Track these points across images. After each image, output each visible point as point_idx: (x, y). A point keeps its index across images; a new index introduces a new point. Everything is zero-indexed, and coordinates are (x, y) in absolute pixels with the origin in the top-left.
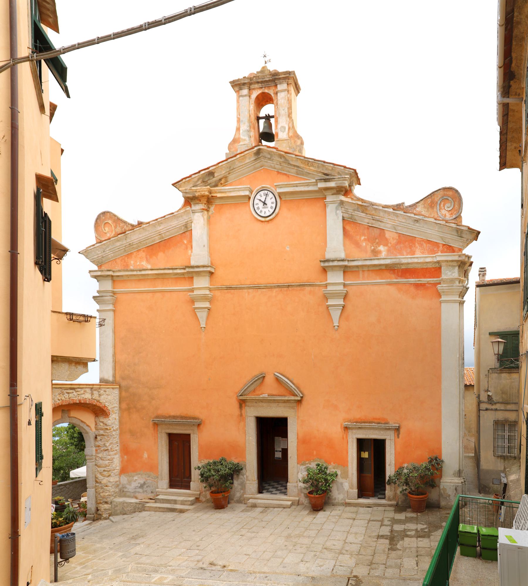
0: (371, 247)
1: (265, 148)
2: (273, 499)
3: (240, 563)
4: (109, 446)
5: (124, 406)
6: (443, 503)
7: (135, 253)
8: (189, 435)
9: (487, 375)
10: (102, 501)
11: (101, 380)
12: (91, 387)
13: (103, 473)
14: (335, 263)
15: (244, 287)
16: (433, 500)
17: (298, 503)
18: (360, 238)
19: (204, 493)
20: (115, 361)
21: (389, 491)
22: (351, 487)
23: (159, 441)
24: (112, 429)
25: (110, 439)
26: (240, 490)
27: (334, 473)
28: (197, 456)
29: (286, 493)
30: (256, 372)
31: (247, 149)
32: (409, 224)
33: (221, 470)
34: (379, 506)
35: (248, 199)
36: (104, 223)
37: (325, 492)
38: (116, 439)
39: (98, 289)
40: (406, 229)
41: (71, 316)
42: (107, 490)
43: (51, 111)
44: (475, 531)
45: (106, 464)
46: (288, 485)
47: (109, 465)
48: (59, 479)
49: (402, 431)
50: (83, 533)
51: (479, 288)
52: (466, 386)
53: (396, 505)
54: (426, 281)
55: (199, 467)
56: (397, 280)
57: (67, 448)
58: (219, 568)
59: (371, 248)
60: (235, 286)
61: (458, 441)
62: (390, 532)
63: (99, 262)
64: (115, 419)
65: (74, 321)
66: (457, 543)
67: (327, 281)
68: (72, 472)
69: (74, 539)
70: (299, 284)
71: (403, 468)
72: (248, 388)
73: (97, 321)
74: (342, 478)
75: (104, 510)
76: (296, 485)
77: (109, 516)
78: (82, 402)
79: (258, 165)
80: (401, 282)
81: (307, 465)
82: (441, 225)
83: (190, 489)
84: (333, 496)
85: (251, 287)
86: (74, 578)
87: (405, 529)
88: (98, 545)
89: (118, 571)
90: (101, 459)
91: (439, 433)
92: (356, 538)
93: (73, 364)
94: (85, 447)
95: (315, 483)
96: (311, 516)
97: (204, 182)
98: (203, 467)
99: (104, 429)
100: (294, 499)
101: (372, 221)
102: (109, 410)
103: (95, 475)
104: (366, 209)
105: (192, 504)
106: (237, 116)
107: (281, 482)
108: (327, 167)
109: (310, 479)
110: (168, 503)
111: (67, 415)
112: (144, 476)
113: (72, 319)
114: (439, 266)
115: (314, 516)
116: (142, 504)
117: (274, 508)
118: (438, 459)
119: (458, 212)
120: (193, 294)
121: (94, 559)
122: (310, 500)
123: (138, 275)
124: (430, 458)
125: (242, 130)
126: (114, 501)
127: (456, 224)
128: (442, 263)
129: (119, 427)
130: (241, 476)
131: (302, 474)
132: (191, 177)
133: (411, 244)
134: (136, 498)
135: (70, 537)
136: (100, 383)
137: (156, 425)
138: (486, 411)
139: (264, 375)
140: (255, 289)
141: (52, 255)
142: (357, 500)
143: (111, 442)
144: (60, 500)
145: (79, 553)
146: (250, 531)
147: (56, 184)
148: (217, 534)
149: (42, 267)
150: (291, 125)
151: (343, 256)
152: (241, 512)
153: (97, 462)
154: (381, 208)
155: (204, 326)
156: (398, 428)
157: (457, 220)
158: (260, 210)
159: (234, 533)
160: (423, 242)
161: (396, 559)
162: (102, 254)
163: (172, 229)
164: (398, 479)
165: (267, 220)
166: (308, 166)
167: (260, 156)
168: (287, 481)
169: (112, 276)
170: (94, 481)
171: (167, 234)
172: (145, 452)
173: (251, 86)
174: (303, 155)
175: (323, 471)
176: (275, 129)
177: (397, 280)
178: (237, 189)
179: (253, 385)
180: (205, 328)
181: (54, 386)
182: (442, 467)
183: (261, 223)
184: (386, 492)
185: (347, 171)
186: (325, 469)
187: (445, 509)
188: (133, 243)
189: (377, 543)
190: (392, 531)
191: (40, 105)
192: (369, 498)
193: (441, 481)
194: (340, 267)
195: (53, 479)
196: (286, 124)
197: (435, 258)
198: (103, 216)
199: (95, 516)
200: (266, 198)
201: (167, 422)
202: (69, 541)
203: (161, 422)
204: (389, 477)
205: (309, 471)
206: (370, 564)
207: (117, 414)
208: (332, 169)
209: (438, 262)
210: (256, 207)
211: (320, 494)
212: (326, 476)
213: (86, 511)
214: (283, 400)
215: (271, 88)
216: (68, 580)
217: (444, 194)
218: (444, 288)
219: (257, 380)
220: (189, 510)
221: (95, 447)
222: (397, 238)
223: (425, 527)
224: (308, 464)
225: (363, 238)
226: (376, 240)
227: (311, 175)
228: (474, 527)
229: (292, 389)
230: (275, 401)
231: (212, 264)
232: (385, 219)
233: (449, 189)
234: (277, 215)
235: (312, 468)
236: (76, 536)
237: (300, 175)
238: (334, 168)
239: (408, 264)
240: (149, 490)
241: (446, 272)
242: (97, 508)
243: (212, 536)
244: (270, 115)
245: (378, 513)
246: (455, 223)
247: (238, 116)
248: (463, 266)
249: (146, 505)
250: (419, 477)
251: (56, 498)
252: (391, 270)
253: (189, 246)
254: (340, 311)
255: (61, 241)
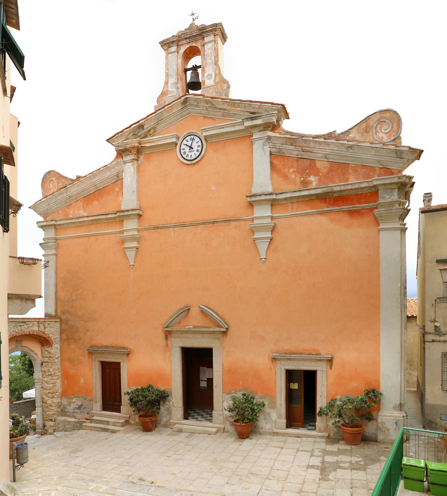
0: (300, 178)
1: (192, 96)
2: (198, 425)
3: (167, 481)
4: (52, 371)
5: (64, 337)
6: (381, 437)
7: (74, 204)
8: (119, 363)
9: (434, 305)
10: (47, 419)
11: (46, 315)
12: (38, 320)
13: (48, 395)
14: (263, 198)
15: (170, 226)
16: (369, 433)
17: (224, 430)
18: (289, 171)
19: (133, 416)
20: (57, 298)
21: (320, 422)
22: (280, 417)
23: (93, 368)
24: (55, 357)
25: (53, 366)
26: (166, 415)
27: (261, 403)
28: (127, 383)
29: (211, 421)
30: (182, 305)
31: (174, 99)
32: (342, 151)
33: (148, 396)
34: (309, 437)
35: (175, 146)
36: (49, 180)
37: (251, 421)
38: (58, 366)
39: (44, 237)
40: (338, 157)
41: (22, 260)
42: (51, 409)
43: (11, 93)
44: (423, 465)
45: (50, 387)
46: (213, 413)
47: (53, 388)
48: (15, 399)
49: (335, 362)
50: (33, 445)
51: (423, 214)
52: (408, 317)
53: (328, 437)
54: (361, 207)
55: (128, 392)
56: (329, 209)
57: (20, 373)
58: (147, 483)
59: (300, 179)
60: (162, 226)
61: (399, 373)
62: (321, 463)
63: (44, 214)
64: (57, 348)
65: (24, 264)
66: (400, 477)
68: (25, 393)
69: (27, 448)
70: (224, 220)
71: (336, 399)
72: (173, 320)
73: (43, 263)
74: (270, 408)
75: (49, 426)
76: (222, 413)
77: (54, 432)
78: (31, 333)
79: (185, 113)
80: (332, 210)
81: (233, 395)
82: (378, 148)
83: (120, 412)
84: (260, 425)
85: (177, 225)
86: (27, 480)
87: (337, 461)
88: (46, 455)
89: (61, 478)
90: (46, 382)
91: (377, 364)
92: (284, 466)
93: (24, 300)
94: (33, 372)
95: (241, 412)
96: (237, 443)
97: (134, 135)
98: (132, 393)
99: (48, 357)
100: (220, 426)
101: (302, 152)
102: (52, 341)
103: (42, 396)
104: (296, 142)
105: (123, 426)
106: (166, 71)
107: (206, 410)
108: (253, 106)
109: (236, 408)
110: (102, 424)
111: (19, 344)
112: (81, 399)
113: (23, 262)
114: (375, 191)
115: (240, 443)
116: (80, 423)
117: (200, 433)
118: (375, 392)
119: (397, 133)
120: (123, 235)
121: (43, 466)
122: (236, 429)
123: (76, 222)
124: (367, 390)
125: (171, 83)
126: (57, 420)
127: (395, 145)
128: (379, 187)
129: (60, 355)
130: (167, 403)
131: (228, 403)
132: (123, 131)
133: (344, 171)
134: (75, 418)
135: (24, 446)
136: (45, 317)
137: (91, 353)
138: (432, 343)
139: (189, 308)
140: (180, 228)
141: (10, 210)
142: (286, 429)
143: (54, 368)
144: (16, 416)
145: (31, 460)
146: (176, 453)
147: (14, 152)
148: (145, 453)
149: (3, 221)
150: (217, 72)
151: (270, 190)
152: (168, 435)
153: (43, 385)
154: (311, 139)
155: (133, 264)
156: (330, 359)
157: (396, 142)
159: (161, 454)
160: (358, 168)
161: (328, 489)
162: (47, 207)
163: (106, 179)
164: (330, 411)
165: (193, 162)
166: (235, 107)
167: (187, 104)
168: (212, 409)
169: (55, 225)
170: (41, 401)
171: (101, 184)
172: (82, 378)
173: (179, 43)
174: (230, 98)
175: (250, 401)
176: (202, 78)
177: (329, 209)
178: (165, 138)
179: (178, 317)
180: (133, 265)
181: (10, 320)
182: (380, 400)
183: (187, 166)
184: (317, 423)
185: (274, 107)
186: (251, 398)
187: (383, 443)
188: (72, 195)
189: (306, 473)
190: (323, 462)
191: (4, 89)
192: (298, 429)
193: (379, 414)
195: (10, 399)
196: (213, 71)
197: (371, 183)
198: (48, 175)
199: (42, 431)
200: (192, 143)
201: (100, 351)
202: (23, 449)
203: (95, 351)
204: (320, 409)
205: (235, 400)
206: (299, 492)
207: (58, 344)
208: (259, 107)
209: (375, 186)
210: (182, 151)
211: (246, 423)
212: (252, 406)
213: (36, 426)
214: (208, 331)
215: (198, 41)
216: (24, 481)
217: (381, 117)
218: (382, 212)
219: (182, 312)
220: (120, 431)
221: (41, 372)
222: (329, 167)
223: (361, 460)
224: (233, 393)
225: (291, 170)
226: (306, 171)
227: (237, 116)
228: (421, 461)
229: (218, 320)
230: (200, 332)
231: (140, 207)
232: (316, 149)
233: (386, 111)
234: (203, 157)
235: (238, 397)
236: (28, 446)
237: (226, 117)
238: (261, 106)
239: (341, 191)
240: (85, 411)
241: (384, 196)
242: (44, 424)
243: (140, 455)
245: (308, 443)
246: (393, 145)
248: (404, 188)
249: (83, 424)
250: (354, 409)
251: (13, 415)
252: (322, 199)
253: (120, 193)
255: (17, 198)
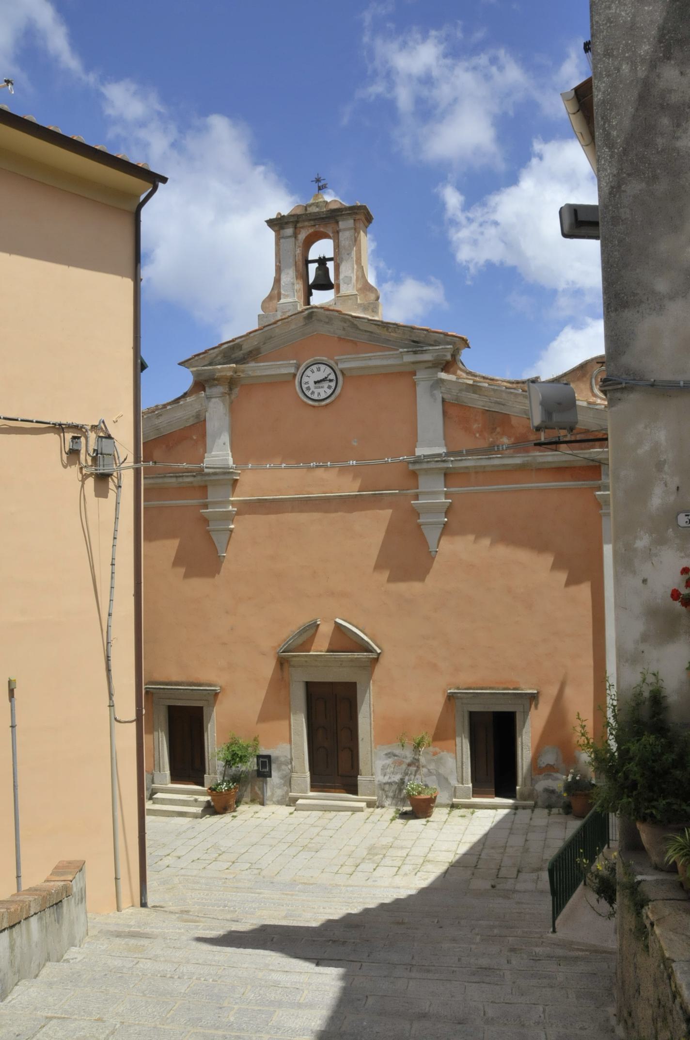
67: (418, 488)
101: (490, 404)
158: (311, 391)
194: (440, 469)
234: (340, 395)
244: (327, 257)
247: (278, 264)
254: (440, 530)
